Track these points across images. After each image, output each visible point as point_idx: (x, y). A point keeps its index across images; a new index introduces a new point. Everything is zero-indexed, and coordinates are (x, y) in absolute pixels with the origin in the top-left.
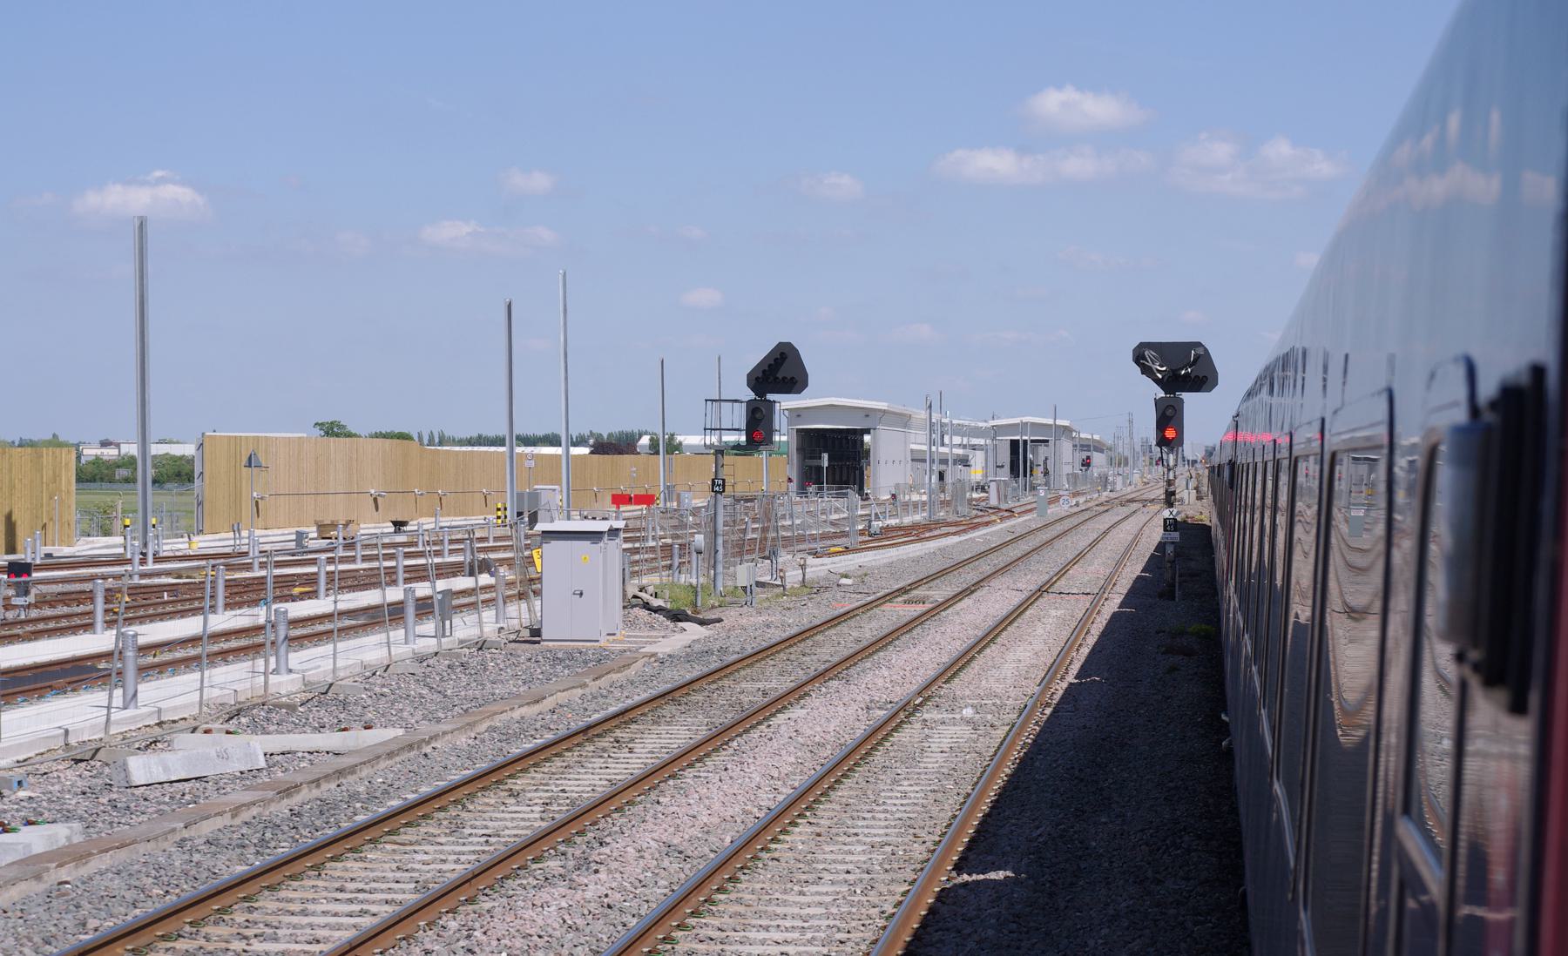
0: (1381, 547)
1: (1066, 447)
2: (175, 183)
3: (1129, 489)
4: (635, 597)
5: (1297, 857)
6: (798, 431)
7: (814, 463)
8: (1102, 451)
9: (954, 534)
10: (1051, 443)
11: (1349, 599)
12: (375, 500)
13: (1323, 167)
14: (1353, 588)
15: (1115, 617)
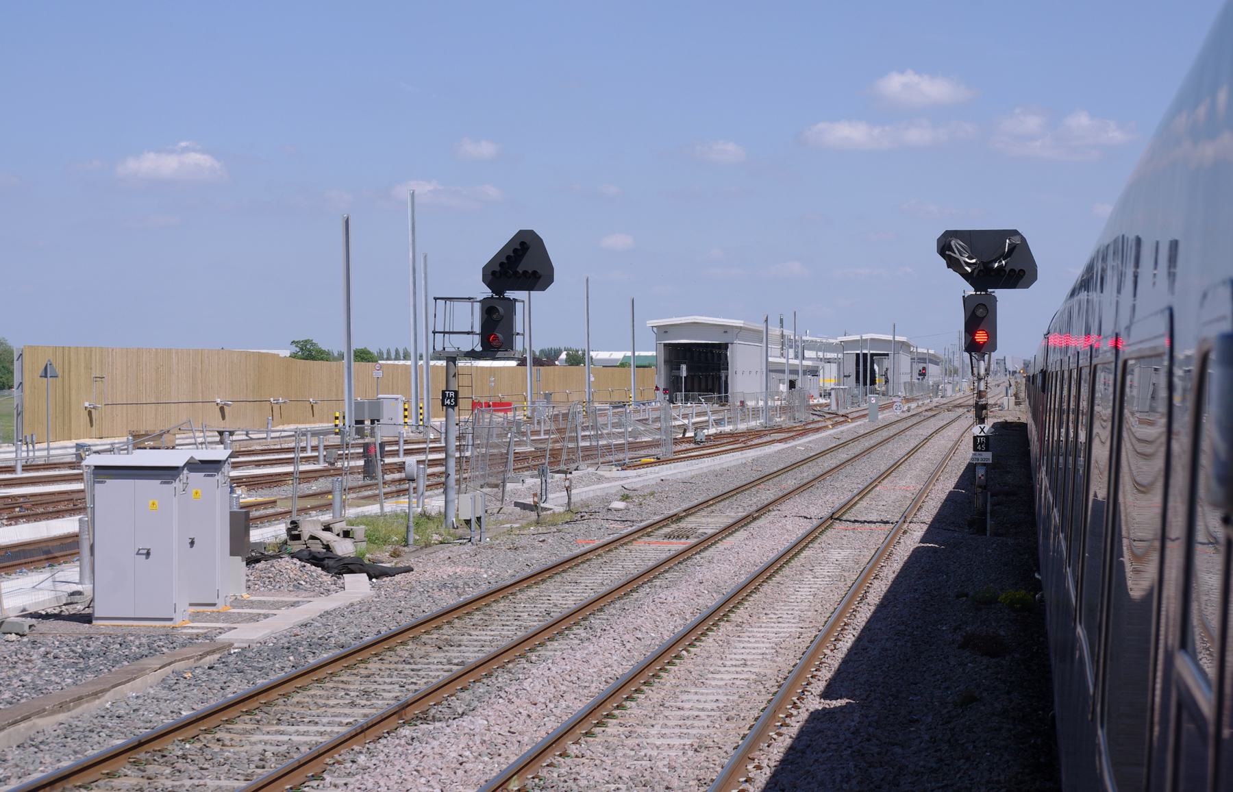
0: (1163, 439)
1: (904, 361)
2: (195, 151)
3: (958, 395)
4: (313, 538)
5: (1095, 686)
6: (665, 345)
7: (675, 373)
8: (937, 364)
9: (780, 441)
10: (891, 356)
11: (1138, 479)
12: (222, 409)
13: (1115, 135)
14: (1141, 467)
15: (916, 554)
